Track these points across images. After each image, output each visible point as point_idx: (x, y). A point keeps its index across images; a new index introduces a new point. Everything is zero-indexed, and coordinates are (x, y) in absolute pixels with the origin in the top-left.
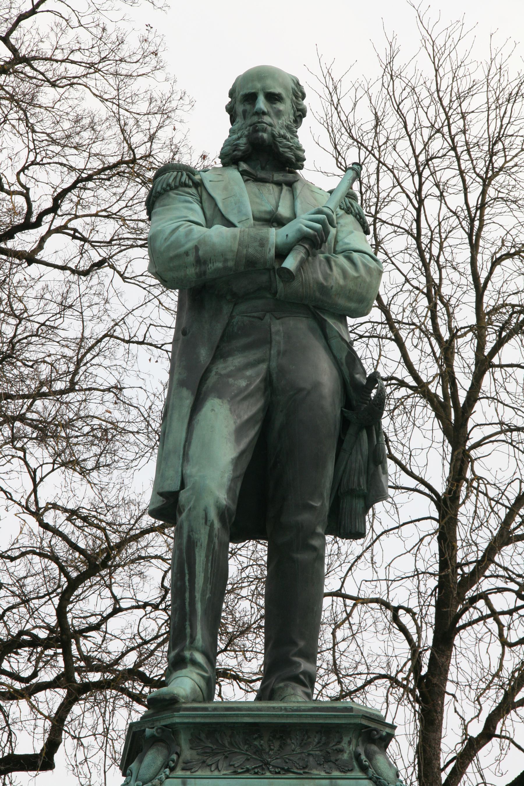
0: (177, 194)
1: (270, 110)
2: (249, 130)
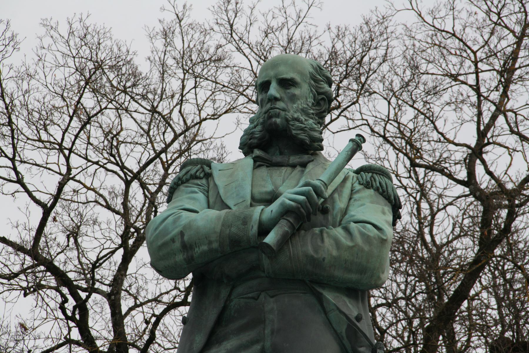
0: (187, 187)
1: (283, 95)
2: (264, 117)
